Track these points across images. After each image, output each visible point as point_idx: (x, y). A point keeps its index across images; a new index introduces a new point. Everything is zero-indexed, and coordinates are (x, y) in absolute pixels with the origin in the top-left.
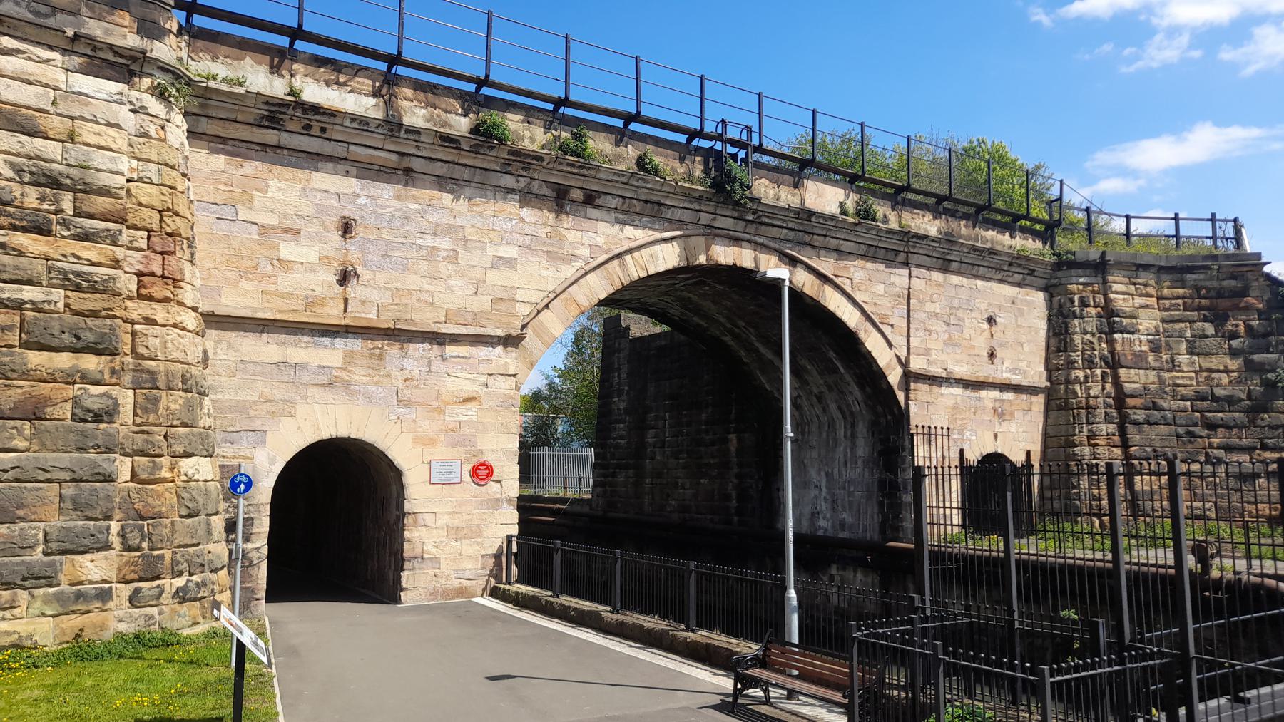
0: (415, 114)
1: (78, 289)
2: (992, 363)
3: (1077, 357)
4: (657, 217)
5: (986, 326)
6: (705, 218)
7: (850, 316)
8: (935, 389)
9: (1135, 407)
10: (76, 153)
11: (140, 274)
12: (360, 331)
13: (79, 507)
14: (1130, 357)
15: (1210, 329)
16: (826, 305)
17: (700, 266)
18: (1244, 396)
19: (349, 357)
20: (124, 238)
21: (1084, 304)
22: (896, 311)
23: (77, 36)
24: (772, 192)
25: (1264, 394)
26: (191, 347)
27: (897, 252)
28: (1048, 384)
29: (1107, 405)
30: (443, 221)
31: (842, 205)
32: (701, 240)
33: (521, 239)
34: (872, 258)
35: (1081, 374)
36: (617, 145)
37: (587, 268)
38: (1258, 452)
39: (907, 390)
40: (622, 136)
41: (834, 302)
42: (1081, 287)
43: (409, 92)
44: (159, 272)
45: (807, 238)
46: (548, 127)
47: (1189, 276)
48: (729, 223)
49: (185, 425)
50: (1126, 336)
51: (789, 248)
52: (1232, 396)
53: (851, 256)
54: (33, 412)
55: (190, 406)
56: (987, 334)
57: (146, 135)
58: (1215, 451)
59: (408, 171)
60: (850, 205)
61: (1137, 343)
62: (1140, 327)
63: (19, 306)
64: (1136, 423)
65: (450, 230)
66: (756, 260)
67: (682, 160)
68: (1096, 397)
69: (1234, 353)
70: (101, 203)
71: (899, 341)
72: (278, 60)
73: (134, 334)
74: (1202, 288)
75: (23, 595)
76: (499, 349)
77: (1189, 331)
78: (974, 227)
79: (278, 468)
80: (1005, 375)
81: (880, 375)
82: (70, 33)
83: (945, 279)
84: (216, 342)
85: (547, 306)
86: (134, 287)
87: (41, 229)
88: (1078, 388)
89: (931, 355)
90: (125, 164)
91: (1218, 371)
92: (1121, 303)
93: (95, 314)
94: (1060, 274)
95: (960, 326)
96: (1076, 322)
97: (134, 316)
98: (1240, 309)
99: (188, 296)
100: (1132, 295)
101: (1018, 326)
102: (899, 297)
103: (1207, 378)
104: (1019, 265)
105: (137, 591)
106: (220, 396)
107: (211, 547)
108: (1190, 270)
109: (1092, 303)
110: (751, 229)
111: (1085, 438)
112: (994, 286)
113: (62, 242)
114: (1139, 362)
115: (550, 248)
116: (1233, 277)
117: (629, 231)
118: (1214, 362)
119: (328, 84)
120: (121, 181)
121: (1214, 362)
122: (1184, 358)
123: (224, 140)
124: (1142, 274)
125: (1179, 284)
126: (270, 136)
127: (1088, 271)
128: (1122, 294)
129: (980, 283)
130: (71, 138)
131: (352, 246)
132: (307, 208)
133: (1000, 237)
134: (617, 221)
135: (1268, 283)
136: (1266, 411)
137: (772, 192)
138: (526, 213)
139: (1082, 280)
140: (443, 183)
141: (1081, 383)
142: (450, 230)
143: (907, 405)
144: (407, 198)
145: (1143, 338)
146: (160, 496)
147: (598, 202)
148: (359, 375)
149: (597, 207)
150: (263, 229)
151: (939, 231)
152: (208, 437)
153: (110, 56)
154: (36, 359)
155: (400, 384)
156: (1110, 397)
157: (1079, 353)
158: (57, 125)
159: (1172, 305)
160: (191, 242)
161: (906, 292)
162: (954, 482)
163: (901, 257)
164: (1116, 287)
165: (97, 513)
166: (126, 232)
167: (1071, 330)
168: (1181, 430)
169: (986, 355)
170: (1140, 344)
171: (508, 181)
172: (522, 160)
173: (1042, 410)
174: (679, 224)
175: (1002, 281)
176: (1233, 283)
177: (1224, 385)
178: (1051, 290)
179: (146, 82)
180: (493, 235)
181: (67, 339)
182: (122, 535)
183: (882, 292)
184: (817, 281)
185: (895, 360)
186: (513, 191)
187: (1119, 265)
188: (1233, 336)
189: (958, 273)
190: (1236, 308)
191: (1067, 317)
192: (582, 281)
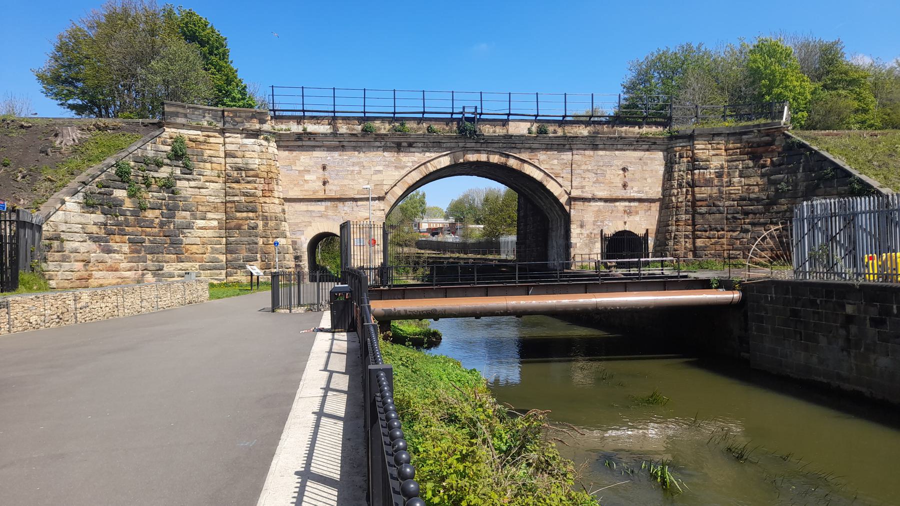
0: (343, 129)
1: (247, 196)
2: (625, 189)
3: (675, 183)
4: (440, 147)
5: (621, 172)
6: (461, 145)
7: (537, 175)
8: (586, 204)
9: (701, 206)
10: (245, 160)
11: (262, 190)
12: (404, 196)
13: (250, 250)
14: (702, 181)
15: (751, 163)
16: (525, 172)
17: (461, 163)
18: (765, 197)
19: (327, 208)
20: (258, 182)
21: (681, 157)
22: (564, 171)
23: (243, 130)
24: (492, 130)
25: (775, 196)
26: (278, 209)
27: (564, 145)
28: (662, 197)
29: (687, 206)
30: (355, 161)
31: (529, 129)
32: (462, 153)
33: (384, 163)
34: (551, 149)
35: (675, 191)
36: (418, 124)
37: (411, 170)
38: (768, 225)
39: (570, 205)
40: (419, 121)
41: (528, 170)
42: (680, 148)
43: (341, 121)
44: (267, 189)
45: (513, 145)
46: (390, 123)
47: (744, 137)
48: (473, 145)
49: (276, 230)
50: (701, 171)
51: (505, 151)
52: (758, 198)
53: (538, 150)
54: (239, 227)
55: (277, 225)
56: (622, 176)
57: (262, 152)
58: (746, 226)
59: (343, 146)
60: (534, 129)
61: (708, 174)
62: (711, 166)
63: (234, 202)
64: (701, 214)
65: (358, 164)
66: (488, 158)
67: (447, 125)
68: (682, 202)
69: (762, 176)
70: (252, 173)
71: (567, 184)
72: (299, 120)
73: (262, 206)
74: (751, 142)
75: (239, 271)
76: (377, 201)
77: (741, 165)
78: (613, 127)
79: (308, 241)
80: (632, 194)
81: (556, 200)
82: (241, 129)
83: (594, 153)
84: (287, 206)
85: (395, 185)
86: (261, 194)
87: (238, 182)
88: (673, 198)
89: (585, 188)
90: (257, 161)
91: (753, 185)
92: (701, 154)
93: (251, 202)
94: (672, 142)
95: (603, 175)
96: (676, 166)
97: (262, 202)
98: (769, 152)
99: (276, 194)
100: (708, 150)
101: (643, 171)
102: (566, 164)
103: (747, 189)
104: (644, 141)
105: (265, 271)
106: (290, 221)
107: (285, 262)
108: (745, 133)
109: (685, 156)
110: (485, 145)
111: (674, 222)
112: (628, 153)
113: (243, 184)
114: (708, 183)
115: (396, 165)
116: (768, 135)
117: (428, 154)
118: (752, 181)
119: (315, 124)
120: (256, 166)
121: (752, 181)
122: (736, 180)
123: (288, 147)
124: (716, 138)
125: (739, 141)
126: (300, 143)
127: (685, 140)
128: (702, 149)
129: (617, 153)
130: (244, 157)
131: (326, 173)
132: (312, 163)
133: (631, 129)
134: (423, 151)
135: (784, 137)
136: (776, 205)
137: (492, 130)
138: (386, 154)
139: (681, 145)
140: (355, 149)
141: (675, 196)
142: (358, 164)
143: (570, 211)
144: (343, 155)
145: (712, 171)
146: (270, 248)
147: (413, 145)
148: (330, 213)
149: (414, 147)
150: (299, 171)
151: (589, 132)
152: (284, 233)
153: (252, 132)
154: (238, 214)
155: (343, 215)
156: (689, 202)
157: (676, 181)
158: (239, 154)
159: (734, 153)
160: (277, 180)
161: (570, 162)
162: (379, 231)
163: (567, 147)
164: (698, 146)
165: (254, 252)
166: (258, 179)
167: (673, 170)
168: (729, 216)
169: (621, 185)
170: (710, 174)
171: (378, 144)
172: (381, 137)
173: (658, 209)
174: (447, 149)
175: (635, 150)
176: (767, 138)
177: (756, 192)
178: (668, 150)
179: (262, 137)
180: (374, 163)
181: (245, 209)
182: (261, 258)
183: (556, 163)
184: (520, 163)
185: (564, 192)
186: (380, 147)
187: (701, 135)
188: (764, 166)
189: (604, 149)
190: (767, 151)
191: (673, 164)
192: (409, 175)
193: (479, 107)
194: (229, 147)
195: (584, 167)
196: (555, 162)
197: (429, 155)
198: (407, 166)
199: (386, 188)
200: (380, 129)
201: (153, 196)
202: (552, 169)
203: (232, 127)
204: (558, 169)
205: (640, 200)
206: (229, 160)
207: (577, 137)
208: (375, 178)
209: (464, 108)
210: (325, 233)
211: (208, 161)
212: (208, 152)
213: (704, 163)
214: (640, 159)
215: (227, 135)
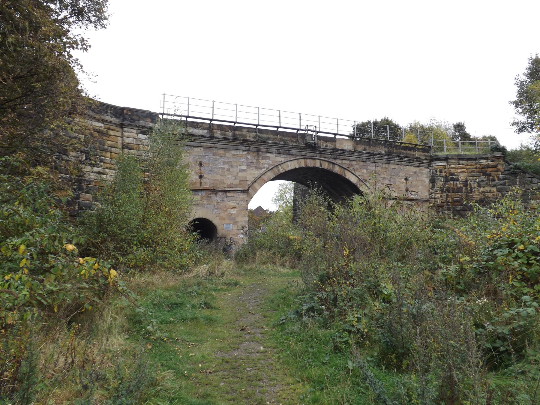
5: (404, 181)
19: (202, 197)
56: (405, 183)
65: (227, 163)
101: (417, 180)
133: (409, 152)
148: (205, 202)
155: (215, 204)
171: (243, 148)
183: (365, 172)
193: (318, 126)
194: (127, 140)
195: (382, 176)
196: (365, 171)
197: (282, 159)
198: (264, 168)
199: (249, 183)
200: (246, 136)
201: (62, 177)
202: (363, 176)
203: (129, 123)
204: (366, 176)
205: (416, 200)
206: (126, 151)
207: (379, 154)
208: (241, 175)
209: (307, 126)
210: (203, 218)
211: (108, 150)
212: (109, 142)
213: (456, 177)
214: (415, 173)
215: (125, 129)
